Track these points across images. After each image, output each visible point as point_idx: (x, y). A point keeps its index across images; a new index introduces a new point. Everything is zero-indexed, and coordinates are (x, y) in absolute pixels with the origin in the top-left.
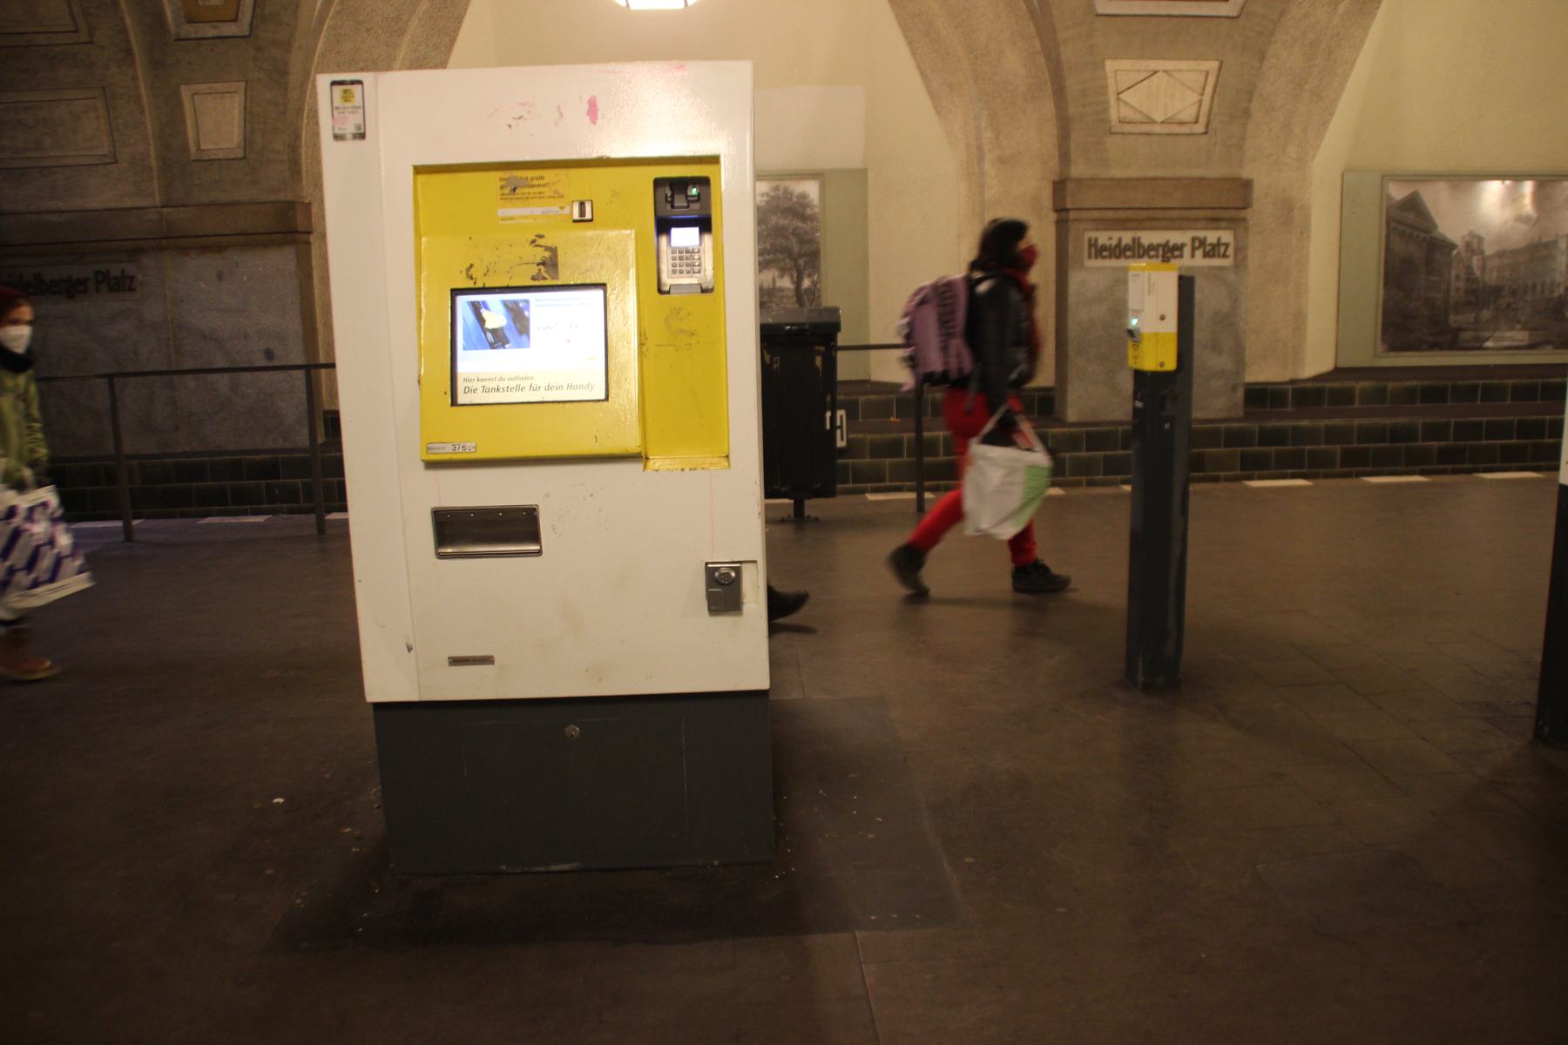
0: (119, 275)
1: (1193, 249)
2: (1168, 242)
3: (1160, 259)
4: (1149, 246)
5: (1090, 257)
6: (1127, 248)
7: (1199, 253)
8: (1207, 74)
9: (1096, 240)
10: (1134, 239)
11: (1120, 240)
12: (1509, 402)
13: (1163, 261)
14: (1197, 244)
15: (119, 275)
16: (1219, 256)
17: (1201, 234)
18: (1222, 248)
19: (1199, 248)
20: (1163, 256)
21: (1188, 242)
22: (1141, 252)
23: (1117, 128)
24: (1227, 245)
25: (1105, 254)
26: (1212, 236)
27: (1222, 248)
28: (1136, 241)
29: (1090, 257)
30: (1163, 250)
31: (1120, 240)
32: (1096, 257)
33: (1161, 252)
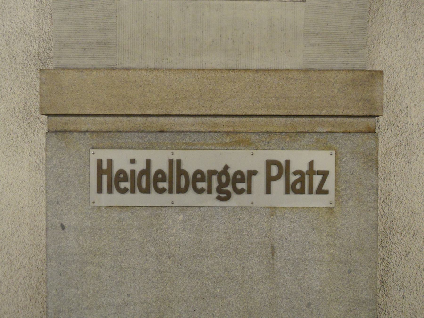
0: (305, 168)
1: (270, 179)
3: (215, 194)
15: (305, 168)
16: (311, 192)
20: (219, 190)
24: (325, 174)
27: (317, 179)
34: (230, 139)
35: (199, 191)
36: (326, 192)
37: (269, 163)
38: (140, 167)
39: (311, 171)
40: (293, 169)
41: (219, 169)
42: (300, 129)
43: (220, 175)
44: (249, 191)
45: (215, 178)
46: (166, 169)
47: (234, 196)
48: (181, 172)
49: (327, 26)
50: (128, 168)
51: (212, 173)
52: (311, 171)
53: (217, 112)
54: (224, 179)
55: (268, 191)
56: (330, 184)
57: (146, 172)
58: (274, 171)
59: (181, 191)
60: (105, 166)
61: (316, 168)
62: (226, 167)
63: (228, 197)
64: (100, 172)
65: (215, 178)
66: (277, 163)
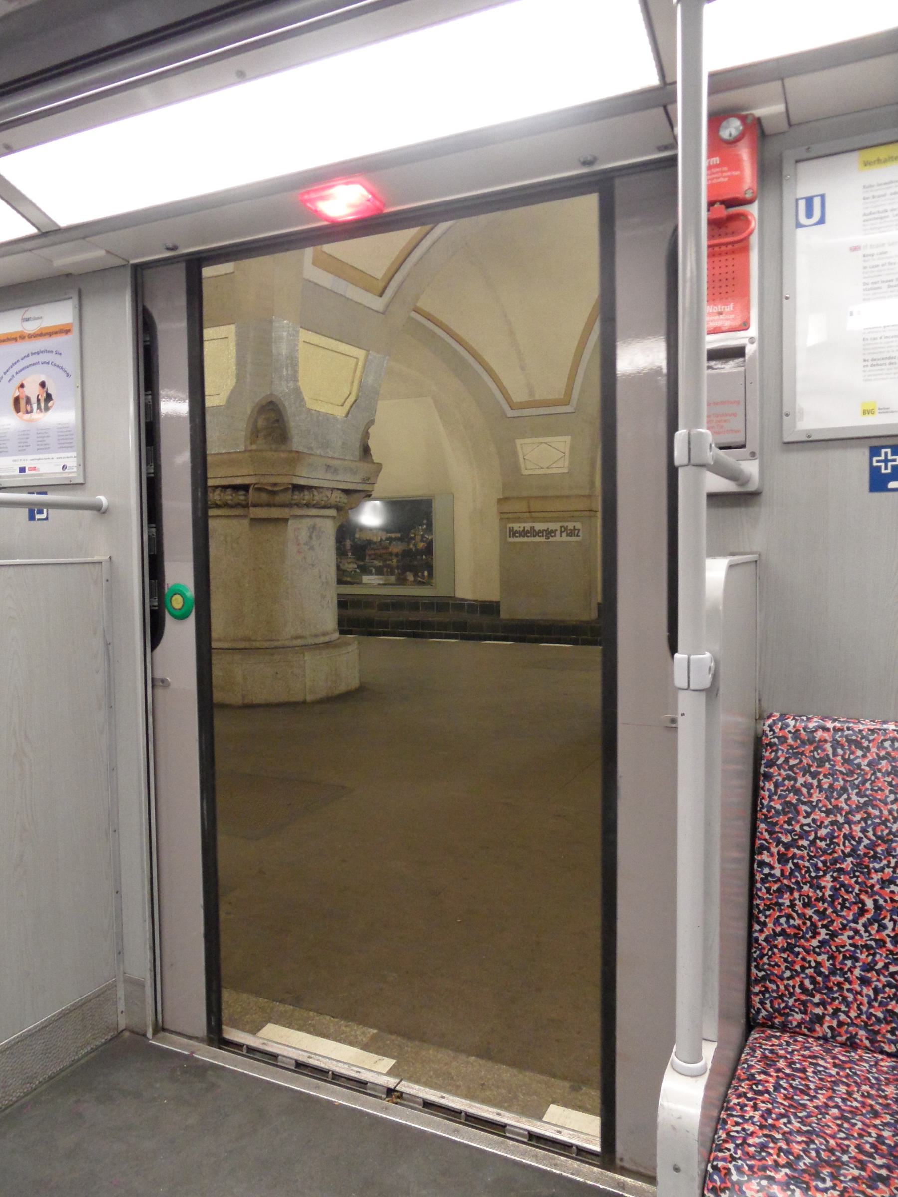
1: (561, 532)
6: (528, 532)
24: (579, 530)
27: (576, 531)
35: (540, 536)
37: (561, 527)
38: (522, 529)
39: (575, 529)
42: (346, 1066)
48: (534, 530)
49: (398, 1100)
50: (518, 529)
51: (544, 530)
52: (575, 529)
56: (580, 534)
57: (524, 530)
58: (563, 529)
59: (534, 536)
63: (548, 538)
64: (510, 531)
66: (563, 526)
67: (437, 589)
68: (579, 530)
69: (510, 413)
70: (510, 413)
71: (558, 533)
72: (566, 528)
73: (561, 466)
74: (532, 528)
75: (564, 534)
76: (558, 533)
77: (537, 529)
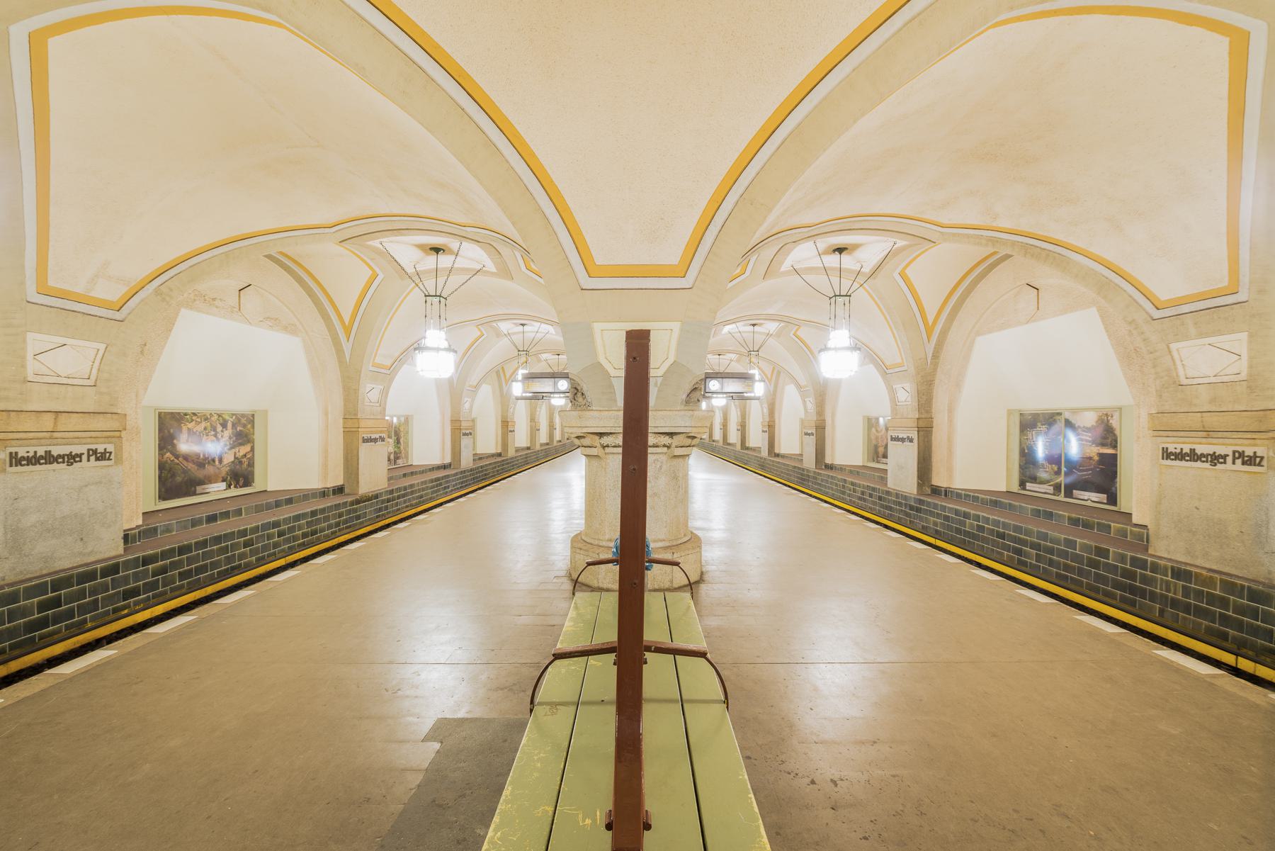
0: (1252, 454)
1: (89, 456)
2: (1215, 453)
3: (66, 464)
4: (1201, 455)
5: (11, 466)
6: (1186, 454)
7: (93, 458)
8: (98, 350)
9: (16, 453)
10: (46, 452)
11: (35, 452)
12: (1095, 531)
13: (68, 465)
14: (1237, 455)
15: (1252, 454)
16: (1255, 465)
17: (93, 447)
18: (108, 455)
19: (1238, 458)
20: (68, 462)
21: (1231, 454)
22: (1196, 458)
23: (1185, 382)
24: (111, 453)
25: (23, 463)
26: (101, 449)
27: (108, 455)
28: (1193, 451)
29: (11, 466)
30: (1211, 458)
31: (35, 452)
32: (16, 466)
33: (1209, 459)
34: (562, 411)
36: (1263, 466)
37: (89, 450)
40: (1246, 454)
41: (1211, 453)
43: (67, 455)
44: (81, 461)
45: (1209, 457)
46: (1189, 452)
47: (1218, 465)
50: (1174, 451)
53: (113, 628)
54: (1213, 457)
55: (1234, 463)
59: (50, 463)
60: (1165, 450)
61: (107, 451)
62: (71, 452)
63: (1215, 465)
65: (1209, 457)
67: (258, 486)
68: (111, 453)
69: (1157, 314)
70: (1157, 314)
71: (1229, 459)
72: (95, 452)
73: (907, 386)
74: (48, 453)
75: (1239, 462)
76: (1229, 459)
77: (55, 453)
